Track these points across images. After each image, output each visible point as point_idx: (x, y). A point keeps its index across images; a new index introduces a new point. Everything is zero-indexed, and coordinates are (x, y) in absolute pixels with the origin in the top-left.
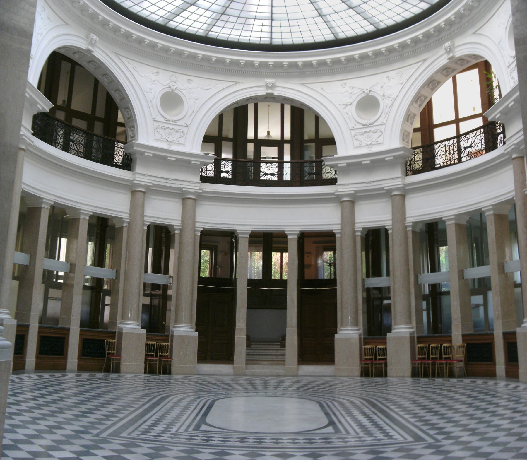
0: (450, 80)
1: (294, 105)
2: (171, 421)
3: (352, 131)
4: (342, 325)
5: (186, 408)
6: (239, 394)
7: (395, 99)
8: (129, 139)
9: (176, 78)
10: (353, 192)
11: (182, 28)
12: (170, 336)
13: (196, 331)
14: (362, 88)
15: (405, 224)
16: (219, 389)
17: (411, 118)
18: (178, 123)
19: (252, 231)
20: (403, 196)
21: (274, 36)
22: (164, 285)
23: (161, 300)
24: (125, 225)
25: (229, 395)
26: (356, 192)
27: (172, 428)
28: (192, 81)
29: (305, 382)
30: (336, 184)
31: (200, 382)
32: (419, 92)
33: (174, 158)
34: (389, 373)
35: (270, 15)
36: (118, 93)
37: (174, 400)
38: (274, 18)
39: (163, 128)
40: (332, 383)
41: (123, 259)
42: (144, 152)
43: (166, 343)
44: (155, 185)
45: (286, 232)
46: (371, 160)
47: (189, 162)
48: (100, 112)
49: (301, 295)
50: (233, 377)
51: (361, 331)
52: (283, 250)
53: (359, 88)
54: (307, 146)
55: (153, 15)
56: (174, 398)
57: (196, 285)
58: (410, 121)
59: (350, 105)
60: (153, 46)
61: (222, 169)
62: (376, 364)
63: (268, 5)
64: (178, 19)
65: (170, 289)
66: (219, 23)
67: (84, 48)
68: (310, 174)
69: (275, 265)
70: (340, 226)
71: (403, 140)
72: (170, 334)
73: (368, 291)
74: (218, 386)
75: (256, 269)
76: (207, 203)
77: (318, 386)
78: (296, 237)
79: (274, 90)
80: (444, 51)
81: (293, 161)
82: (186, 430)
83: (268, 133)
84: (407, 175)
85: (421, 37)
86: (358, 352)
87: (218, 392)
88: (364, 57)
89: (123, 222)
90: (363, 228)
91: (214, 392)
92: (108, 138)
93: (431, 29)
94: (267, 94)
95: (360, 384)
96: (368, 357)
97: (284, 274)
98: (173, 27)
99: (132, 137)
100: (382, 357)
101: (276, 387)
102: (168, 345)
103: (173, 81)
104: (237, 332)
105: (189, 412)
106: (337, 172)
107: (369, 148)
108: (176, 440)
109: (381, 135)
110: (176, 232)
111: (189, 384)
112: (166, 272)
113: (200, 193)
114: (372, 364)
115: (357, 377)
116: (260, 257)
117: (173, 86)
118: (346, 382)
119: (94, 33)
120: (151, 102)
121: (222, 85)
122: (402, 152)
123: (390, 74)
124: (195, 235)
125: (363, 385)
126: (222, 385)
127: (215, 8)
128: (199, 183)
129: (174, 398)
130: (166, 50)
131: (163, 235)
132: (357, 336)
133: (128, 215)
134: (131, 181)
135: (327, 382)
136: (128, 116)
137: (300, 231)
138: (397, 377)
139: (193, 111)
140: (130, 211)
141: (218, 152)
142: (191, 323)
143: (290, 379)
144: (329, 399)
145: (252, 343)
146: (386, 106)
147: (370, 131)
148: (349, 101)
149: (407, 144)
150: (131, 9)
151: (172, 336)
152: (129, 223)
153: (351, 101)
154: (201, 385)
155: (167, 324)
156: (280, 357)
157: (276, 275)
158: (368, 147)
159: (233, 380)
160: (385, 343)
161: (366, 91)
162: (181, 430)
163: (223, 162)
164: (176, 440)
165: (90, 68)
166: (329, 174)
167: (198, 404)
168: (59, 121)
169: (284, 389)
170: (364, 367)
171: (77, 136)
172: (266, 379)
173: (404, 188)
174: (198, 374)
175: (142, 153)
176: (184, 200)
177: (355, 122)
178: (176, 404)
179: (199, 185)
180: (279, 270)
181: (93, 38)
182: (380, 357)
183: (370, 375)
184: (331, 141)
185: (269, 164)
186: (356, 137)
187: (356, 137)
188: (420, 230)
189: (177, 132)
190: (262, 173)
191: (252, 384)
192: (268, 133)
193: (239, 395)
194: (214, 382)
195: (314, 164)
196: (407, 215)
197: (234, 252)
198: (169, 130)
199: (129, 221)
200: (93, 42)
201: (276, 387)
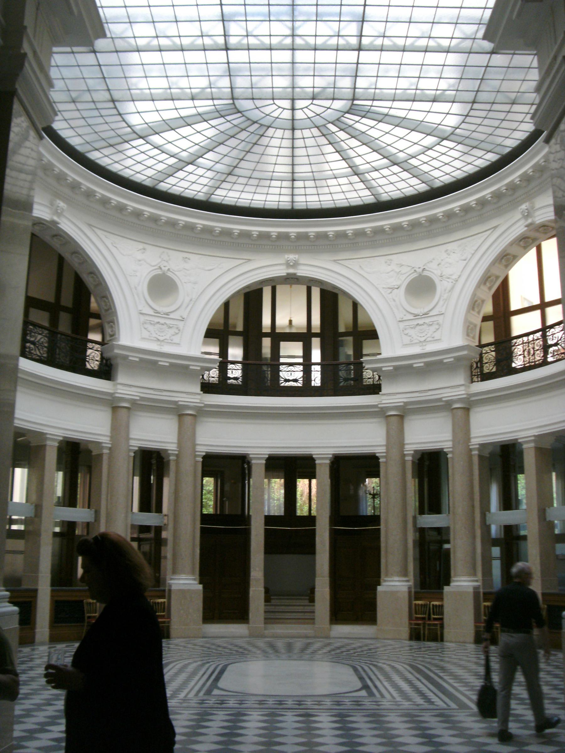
0: (533, 251)
1: (323, 288)
2: (176, 687)
3: (401, 324)
4: (387, 575)
5: (194, 673)
6: (257, 657)
7: (457, 281)
8: (108, 338)
9: (169, 256)
10: (402, 404)
11: (176, 190)
12: (167, 591)
13: (200, 583)
14: (413, 266)
15: (469, 446)
16: (232, 653)
17: (478, 305)
18: (172, 316)
19: (269, 454)
20: (467, 410)
21: (297, 169)
22: (156, 527)
23: (153, 545)
24: (106, 451)
25: (245, 659)
26: (406, 404)
27: (179, 694)
28: (189, 259)
29: (338, 644)
30: (380, 393)
31: (208, 645)
32: (488, 270)
33: (198, 366)
34: (447, 636)
35: (290, 175)
36: (92, 277)
37: (178, 667)
38: (295, 178)
39: (152, 322)
40: (372, 647)
41: (104, 497)
42: (128, 356)
43: (162, 600)
44: (142, 399)
45: (314, 456)
46: (424, 363)
47: (186, 367)
48: (67, 300)
49: (334, 535)
50: (248, 639)
51: (411, 583)
52: (310, 475)
53: (409, 266)
54: (342, 340)
55: (138, 175)
56: (177, 664)
57: (198, 525)
58: (476, 310)
59: (397, 288)
60: (138, 214)
61: (228, 375)
62: (429, 625)
63: (288, 163)
64: (171, 180)
65: (165, 530)
66: (224, 185)
67: (48, 219)
68: (346, 380)
69: (302, 495)
70: (385, 448)
71: (468, 335)
72: (167, 588)
73: (422, 531)
74: (231, 649)
75: (275, 501)
76: (213, 420)
77: (354, 649)
78: (328, 462)
79: (297, 270)
80: (520, 216)
81: (324, 363)
82: (197, 695)
83: (290, 322)
84: (472, 382)
85: (488, 197)
86: (406, 609)
87: (231, 656)
88: (415, 224)
89: (103, 448)
90: (416, 451)
91: (226, 657)
92: (78, 337)
93: (502, 186)
94: (288, 274)
95: (408, 648)
96: (420, 616)
97: (314, 506)
98: (165, 190)
99: (111, 336)
100: (438, 617)
101: (303, 650)
102: (164, 602)
103: (164, 260)
104: (252, 583)
105: (197, 678)
106: (381, 378)
107: (422, 346)
108: (185, 705)
109: (438, 329)
110: (172, 458)
111: (193, 649)
112: (159, 509)
113: (201, 407)
114: (424, 624)
115: (405, 640)
116: (281, 486)
117: (165, 267)
118: (391, 645)
119: (60, 199)
120: (136, 288)
121: (228, 264)
122: (465, 352)
123: (450, 247)
124: (196, 462)
125: (411, 650)
126: (236, 648)
127: (219, 167)
128: (199, 394)
129: (177, 664)
130: (155, 219)
131: (154, 461)
132: (405, 589)
133: (108, 439)
134: (111, 394)
135: (366, 645)
136: (105, 308)
137: (333, 454)
138: (456, 642)
139: (191, 300)
140: (111, 433)
141: (223, 353)
142: (193, 573)
143: (321, 641)
144: (366, 663)
145: (272, 597)
146: (445, 290)
147: (424, 323)
148: (396, 283)
149: (473, 340)
150: (109, 168)
151: (170, 591)
152: (110, 449)
153: (399, 283)
154: (209, 649)
155: (162, 576)
156: (308, 614)
157: (302, 509)
158: (421, 344)
159: (249, 643)
160: (442, 599)
161: (418, 270)
162: (191, 695)
163: (230, 366)
164: (185, 705)
165: (56, 244)
166: (371, 380)
167: (208, 669)
168: (62, 334)
169: (312, 652)
170: (414, 628)
171: (39, 337)
172: (290, 641)
173: (468, 398)
174: (203, 637)
175: (125, 357)
176: (181, 416)
177: (405, 313)
178: (181, 671)
179: (199, 397)
180: (307, 502)
181: (59, 205)
182: (436, 617)
183: (422, 638)
184: (372, 334)
185: (291, 367)
186: (406, 332)
187: (406, 332)
188: (490, 454)
189: (170, 327)
190: (282, 379)
191: (272, 646)
192: (290, 322)
193: (255, 659)
194: (225, 645)
195: (352, 367)
196: (472, 435)
197: (247, 482)
198: (160, 326)
199: (110, 446)
200: (59, 211)
201: (303, 650)
